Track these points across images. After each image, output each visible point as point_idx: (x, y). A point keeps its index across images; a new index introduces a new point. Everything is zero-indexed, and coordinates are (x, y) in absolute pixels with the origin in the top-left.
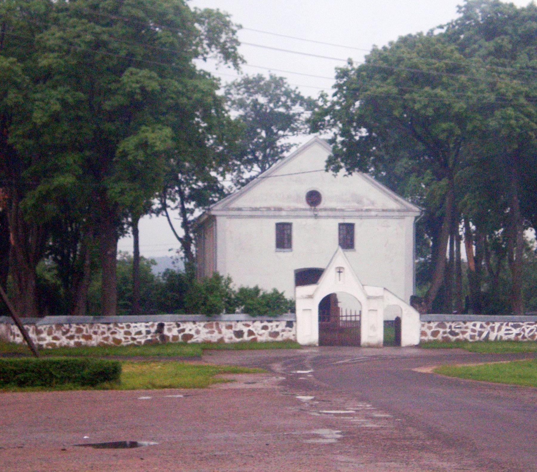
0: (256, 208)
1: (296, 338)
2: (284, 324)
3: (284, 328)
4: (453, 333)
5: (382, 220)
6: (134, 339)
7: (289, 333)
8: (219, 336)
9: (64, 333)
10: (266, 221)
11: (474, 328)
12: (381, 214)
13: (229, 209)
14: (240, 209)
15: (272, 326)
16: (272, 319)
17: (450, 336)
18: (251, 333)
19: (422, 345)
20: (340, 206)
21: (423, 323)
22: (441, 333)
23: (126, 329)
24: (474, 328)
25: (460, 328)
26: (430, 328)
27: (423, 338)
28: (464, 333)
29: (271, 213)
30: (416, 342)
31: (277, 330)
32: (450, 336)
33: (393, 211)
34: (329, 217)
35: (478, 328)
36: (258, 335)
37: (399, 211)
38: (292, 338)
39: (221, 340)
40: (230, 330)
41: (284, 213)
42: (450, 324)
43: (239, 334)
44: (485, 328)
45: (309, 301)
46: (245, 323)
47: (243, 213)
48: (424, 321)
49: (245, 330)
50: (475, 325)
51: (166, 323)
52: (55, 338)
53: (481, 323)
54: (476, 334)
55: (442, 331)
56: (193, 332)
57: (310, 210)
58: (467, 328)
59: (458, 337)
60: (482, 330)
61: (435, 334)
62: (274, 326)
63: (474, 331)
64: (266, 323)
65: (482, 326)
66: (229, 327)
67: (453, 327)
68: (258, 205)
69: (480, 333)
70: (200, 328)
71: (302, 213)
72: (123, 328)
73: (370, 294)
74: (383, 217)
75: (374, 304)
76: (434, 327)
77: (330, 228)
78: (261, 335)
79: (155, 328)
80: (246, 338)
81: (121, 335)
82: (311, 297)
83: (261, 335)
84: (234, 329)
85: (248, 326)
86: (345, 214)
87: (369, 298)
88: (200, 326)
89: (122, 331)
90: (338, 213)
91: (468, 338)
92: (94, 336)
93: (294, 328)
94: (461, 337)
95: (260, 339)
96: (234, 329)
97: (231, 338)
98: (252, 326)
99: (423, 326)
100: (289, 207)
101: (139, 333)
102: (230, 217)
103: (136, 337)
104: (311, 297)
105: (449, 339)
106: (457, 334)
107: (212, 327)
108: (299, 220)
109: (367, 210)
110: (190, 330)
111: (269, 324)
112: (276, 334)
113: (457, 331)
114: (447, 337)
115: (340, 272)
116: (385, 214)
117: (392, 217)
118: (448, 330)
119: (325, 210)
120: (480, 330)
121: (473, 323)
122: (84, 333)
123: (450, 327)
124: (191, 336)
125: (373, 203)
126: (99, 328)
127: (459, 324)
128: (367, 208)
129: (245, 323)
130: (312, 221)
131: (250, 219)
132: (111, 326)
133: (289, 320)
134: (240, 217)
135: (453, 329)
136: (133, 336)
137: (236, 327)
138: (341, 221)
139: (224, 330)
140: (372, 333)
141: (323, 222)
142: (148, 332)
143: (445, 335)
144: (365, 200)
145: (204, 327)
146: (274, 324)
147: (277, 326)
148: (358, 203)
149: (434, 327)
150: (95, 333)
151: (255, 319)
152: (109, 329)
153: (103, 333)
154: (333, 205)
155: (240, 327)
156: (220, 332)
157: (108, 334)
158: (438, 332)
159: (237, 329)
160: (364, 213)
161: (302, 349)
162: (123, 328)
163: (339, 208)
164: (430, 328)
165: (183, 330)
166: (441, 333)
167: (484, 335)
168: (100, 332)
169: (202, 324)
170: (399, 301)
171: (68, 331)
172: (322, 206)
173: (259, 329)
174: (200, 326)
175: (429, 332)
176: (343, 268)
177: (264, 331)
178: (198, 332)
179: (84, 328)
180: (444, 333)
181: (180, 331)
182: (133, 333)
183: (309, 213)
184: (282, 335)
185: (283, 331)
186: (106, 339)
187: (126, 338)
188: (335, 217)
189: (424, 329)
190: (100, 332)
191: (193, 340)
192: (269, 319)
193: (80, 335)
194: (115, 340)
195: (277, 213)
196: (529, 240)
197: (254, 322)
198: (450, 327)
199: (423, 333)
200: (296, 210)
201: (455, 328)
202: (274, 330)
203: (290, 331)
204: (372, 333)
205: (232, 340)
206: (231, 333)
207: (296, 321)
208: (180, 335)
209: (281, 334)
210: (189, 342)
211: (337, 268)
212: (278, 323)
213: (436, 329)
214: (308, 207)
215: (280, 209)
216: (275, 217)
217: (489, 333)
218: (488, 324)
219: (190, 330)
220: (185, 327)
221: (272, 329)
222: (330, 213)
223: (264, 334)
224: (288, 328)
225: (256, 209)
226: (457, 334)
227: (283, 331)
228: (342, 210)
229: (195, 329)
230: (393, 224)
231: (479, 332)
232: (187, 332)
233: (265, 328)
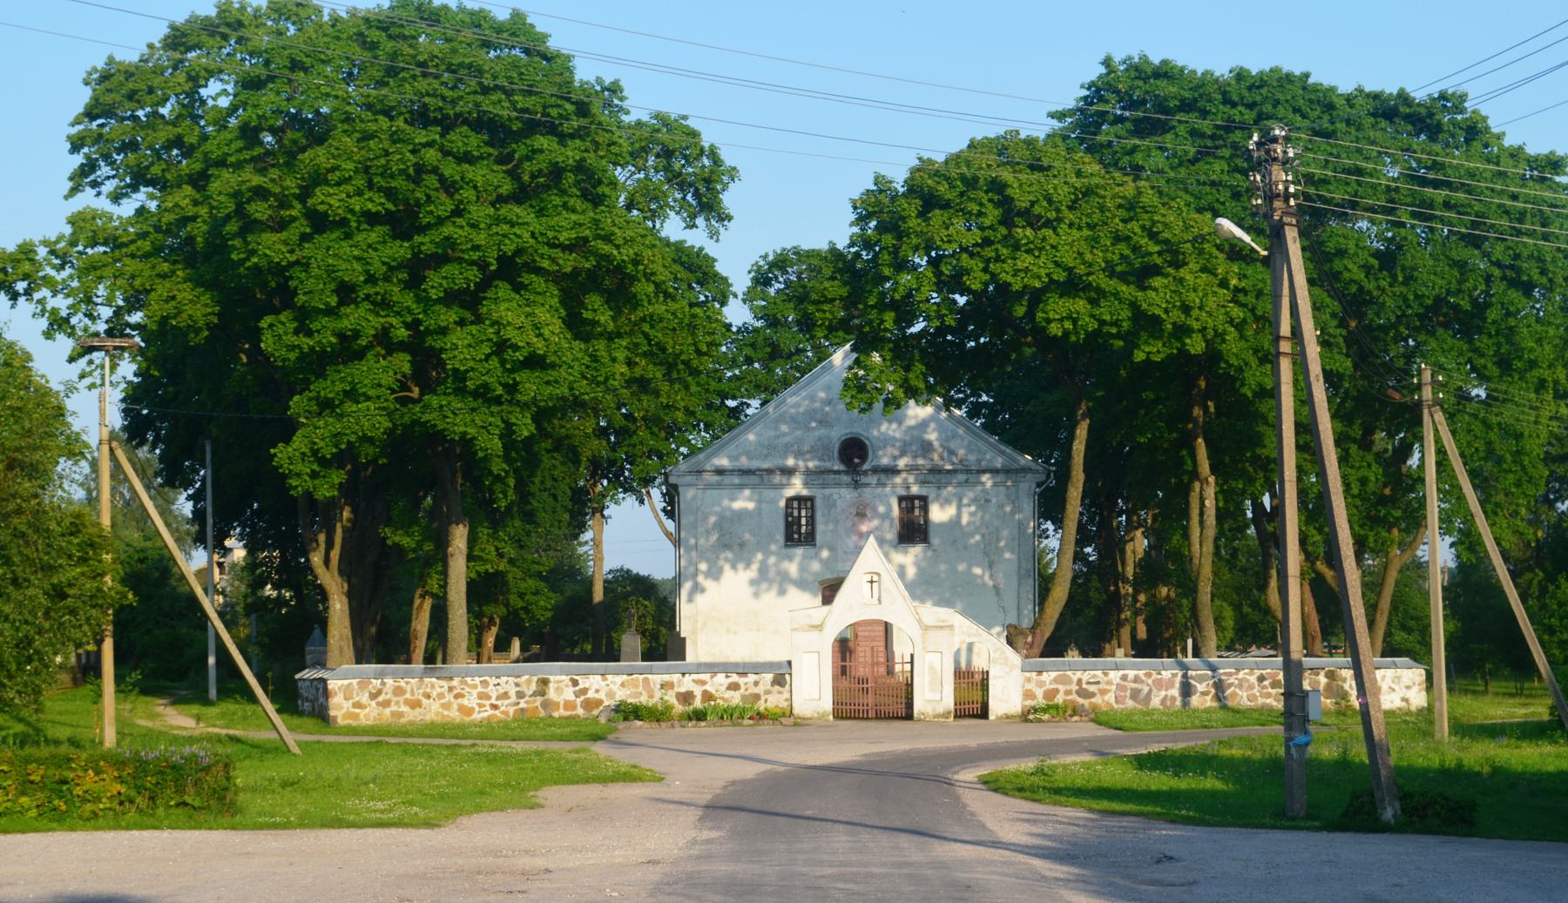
6: (495, 707)
9: (373, 696)
17: (1081, 701)
19: (1025, 717)
23: (480, 689)
26: (1041, 684)
28: (1103, 692)
32: (1081, 701)
42: (1079, 674)
45: (815, 634)
51: (552, 678)
52: (358, 705)
55: (1062, 688)
57: (846, 473)
72: (475, 687)
73: (928, 621)
79: (533, 687)
81: (471, 701)
82: (819, 627)
87: (926, 628)
89: (475, 693)
92: (425, 701)
96: (677, 689)
101: (505, 695)
103: (499, 703)
104: (819, 627)
106: (1093, 695)
111: (742, 681)
113: (1092, 688)
122: (408, 696)
123: (1079, 682)
126: (433, 687)
132: (455, 682)
136: (493, 701)
140: (934, 695)
142: (520, 695)
145: (623, 685)
150: (428, 696)
152: (451, 689)
153: (441, 696)
157: (449, 697)
159: (683, 690)
161: (1033, 847)
162: (475, 687)
164: (1041, 684)
165: (584, 691)
168: (434, 694)
171: (379, 692)
175: (1039, 693)
177: (731, 693)
179: (408, 688)
181: (577, 695)
182: (494, 696)
183: (846, 479)
185: (768, 692)
186: (447, 706)
187: (480, 706)
189: (1028, 686)
190: (434, 694)
193: (401, 699)
194: (461, 708)
196: (55, 385)
198: (1079, 682)
199: (1028, 695)
204: (934, 695)
208: (579, 701)
224: (777, 688)
226: (1093, 695)
227: (768, 692)
232: (591, 694)
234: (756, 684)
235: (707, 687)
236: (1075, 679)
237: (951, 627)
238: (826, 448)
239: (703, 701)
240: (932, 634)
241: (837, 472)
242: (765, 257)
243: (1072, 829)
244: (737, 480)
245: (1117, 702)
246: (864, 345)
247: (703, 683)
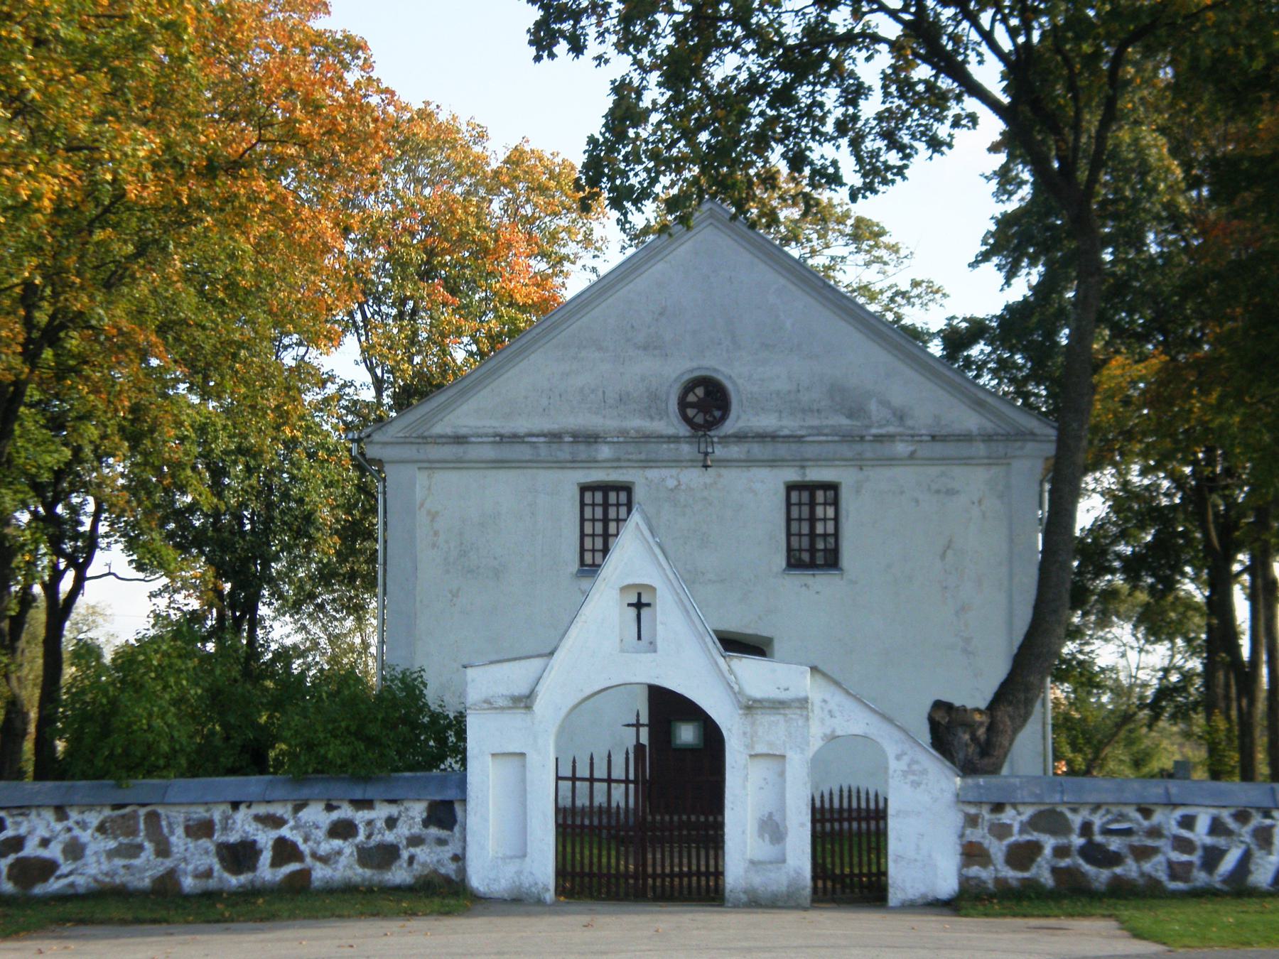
0: (515, 436)
1: (462, 871)
2: (418, 810)
3: (417, 830)
4: (1094, 853)
5: (934, 471)
7: (439, 849)
8: (162, 866)
10: (546, 477)
11: (1185, 833)
12: (925, 450)
13: (425, 440)
14: (460, 440)
15: (370, 823)
16: (370, 792)
18: (285, 851)
20: (789, 424)
21: (972, 810)
22: (1047, 851)
24: (1185, 833)
25: (1128, 832)
26: (1001, 831)
27: (975, 871)
28: (1142, 853)
29: (565, 452)
30: (947, 885)
31: (390, 837)
33: (967, 438)
34: (750, 462)
35: (1200, 833)
36: (314, 855)
37: (988, 438)
38: (449, 869)
39: (170, 877)
40: (205, 843)
41: (605, 452)
43: (240, 856)
44: (1228, 833)
45: (517, 719)
46: (262, 810)
47: (473, 452)
48: (978, 804)
49: (265, 838)
50: (1188, 822)
53: (1214, 811)
54: (1195, 858)
55: (1049, 843)
56: (54, 852)
57: (688, 440)
58: (1155, 832)
59: (1118, 870)
60: (1221, 842)
61: (1022, 855)
62: (380, 824)
63: (1183, 845)
64: (346, 812)
65: (1217, 827)
66: (201, 829)
67: (1096, 828)
68: (521, 425)
69: (1212, 857)
70: (85, 836)
71: (665, 449)
74: (932, 461)
75: (772, 731)
76: (1016, 828)
77: (759, 495)
78: (325, 860)
80: (266, 872)
82: (524, 702)
83: (325, 860)
84: (218, 837)
85: (275, 822)
86: (809, 451)
87: (751, 707)
88: (86, 825)
90: (782, 450)
91: (1162, 876)
93: (457, 828)
94: (1130, 869)
95: (320, 873)
97: (208, 874)
98: (292, 823)
99: (972, 821)
100: (623, 433)
102: (431, 465)
105: (1084, 875)
106: (1114, 859)
107: (134, 832)
108: (653, 474)
109: (879, 438)
110: (45, 843)
111: (360, 817)
112: (388, 854)
113: (1115, 844)
114: (1071, 872)
115: (639, 605)
116: (939, 449)
117: (966, 461)
118: (1078, 841)
119: (740, 437)
120: (1209, 840)
121: (1179, 813)
123: (1086, 829)
124: (47, 868)
125: (901, 417)
127: (1121, 817)
128: (883, 431)
129: (262, 810)
130: (693, 477)
131: (493, 472)
133: (438, 798)
134: (459, 464)
135: (1098, 838)
137: (225, 828)
138: (793, 475)
139: (178, 840)
141: (735, 479)
143: (1064, 863)
144: (873, 406)
145: (101, 828)
146: (381, 812)
147: (391, 823)
148: (850, 416)
149: (1016, 828)
151: (305, 792)
154: (767, 422)
155: (243, 825)
156: (163, 850)
158: (1036, 848)
159: (233, 838)
160: (865, 440)
163: (786, 432)
164: (1001, 831)
166: (1047, 851)
167: (1228, 863)
169: (94, 819)
170: (874, 719)
172: (730, 427)
173: (320, 834)
174: (83, 825)
175: (997, 849)
176: (652, 589)
177: (337, 843)
178: (75, 850)
180: (1061, 852)
183: (686, 449)
184: (411, 859)
185: (415, 841)
188: (772, 463)
189: (975, 835)
191: (54, 885)
192: (358, 794)
195: (582, 451)
197: (298, 808)
198: (1086, 829)
199: (972, 854)
200: (646, 438)
201: (1106, 832)
202: (377, 838)
203: (441, 842)
205: (212, 884)
206: (207, 852)
207: (464, 801)
209: (405, 854)
210: (39, 890)
211: (625, 589)
212: (393, 810)
213: (1027, 837)
214: (684, 430)
215: (591, 438)
216: (574, 463)
217: (1246, 858)
218: (1242, 816)
219: (45, 843)
220: (23, 830)
221: (369, 837)
222: (757, 450)
223: (339, 853)
224: (434, 831)
225: (515, 438)
227: (415, 841)
228: (798, 439)
229: (65, 837)
230: (974, 481)
231: (1206, 849)
232: (31, 849)
233: (343, 830)
234: (391, 823)
235: (285, 832)
236: (1076, 820)
237: (803, 703)
238: (654, 397)
239: (276, 862)
240: (764, 719)
241: (674, 439)
242: (529, 31)
243: (1093, 911)
244: (489, 452)
245: (1173, 877)
246: (702, 172)
247: (278, 822)
